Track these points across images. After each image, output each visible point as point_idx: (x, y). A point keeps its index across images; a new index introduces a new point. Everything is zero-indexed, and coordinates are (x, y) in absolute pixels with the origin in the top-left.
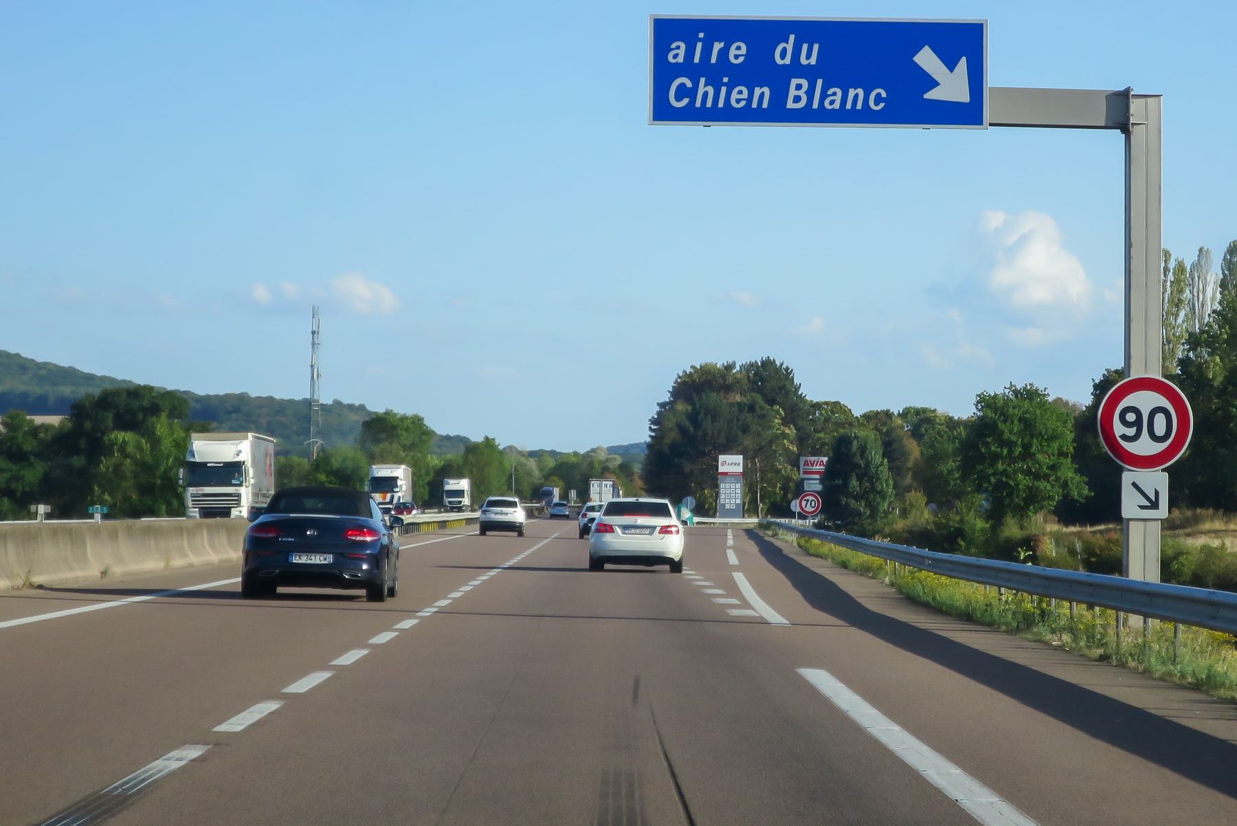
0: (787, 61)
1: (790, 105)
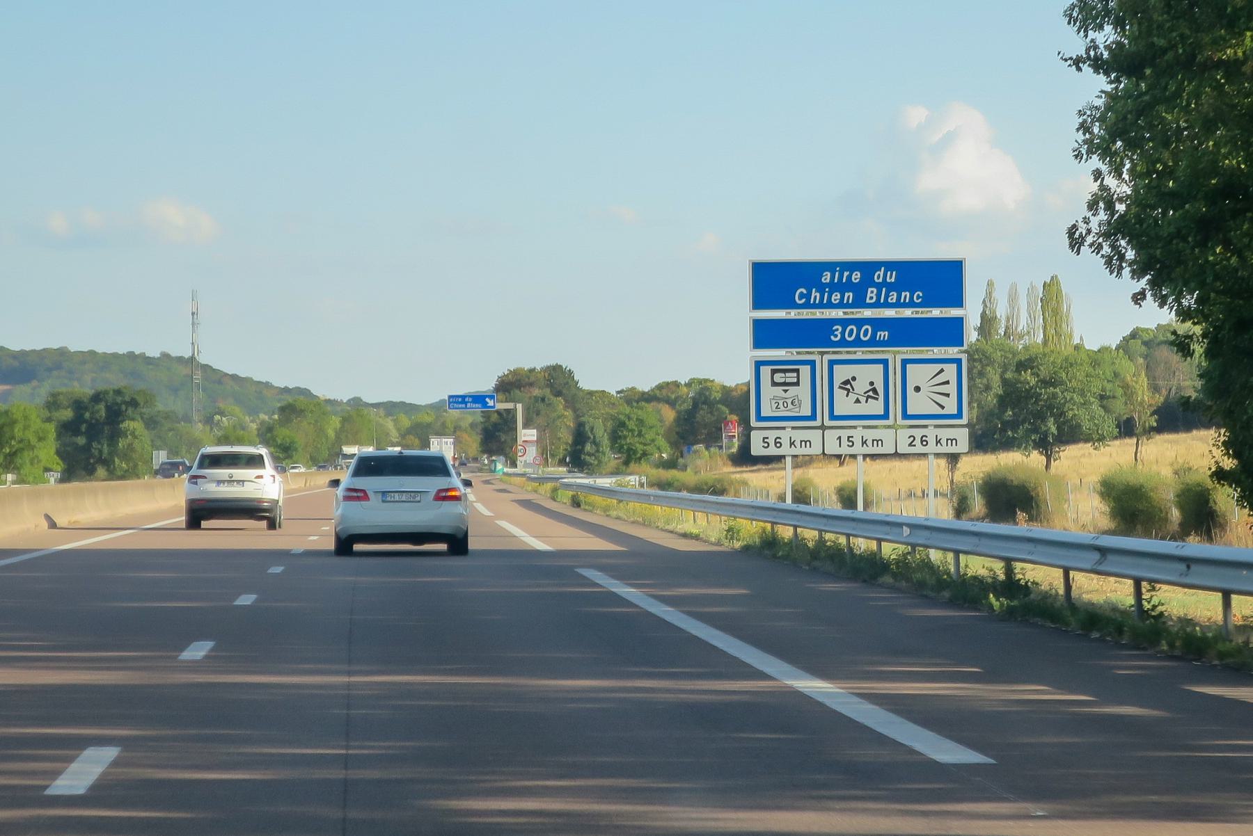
1: (868, 301)
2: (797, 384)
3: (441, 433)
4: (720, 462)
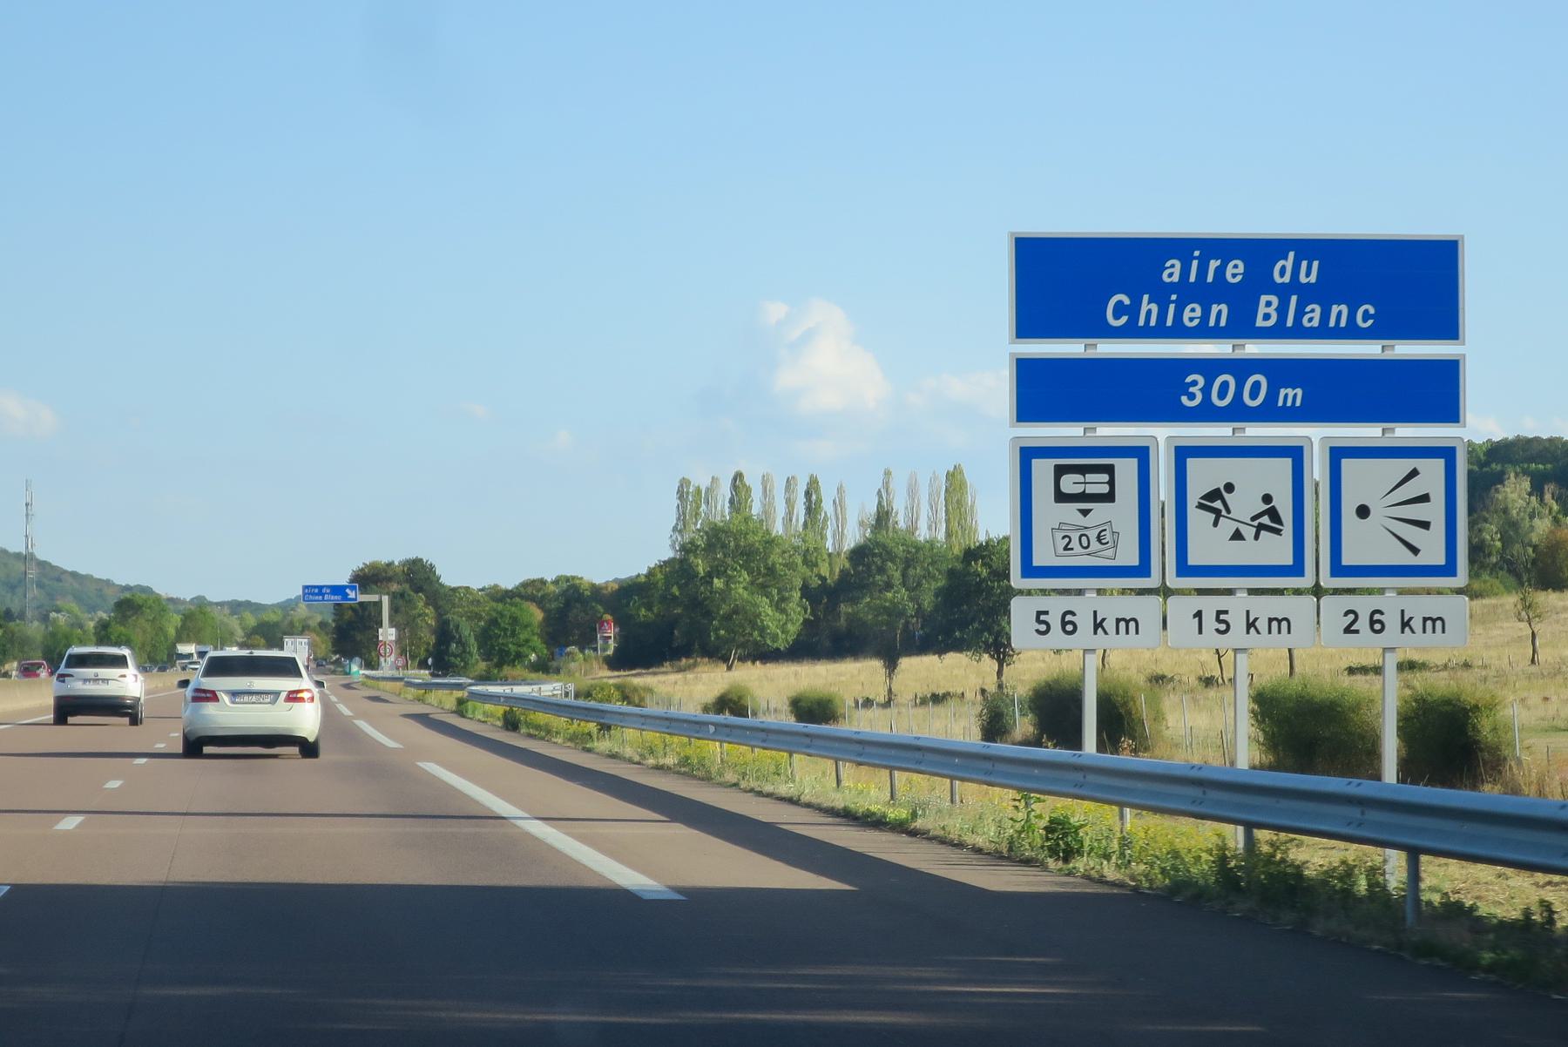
0: (1287, 279)
1: (1260, 323)
2: (1109, 497)
3: (292, 631)
4: (595, 665)
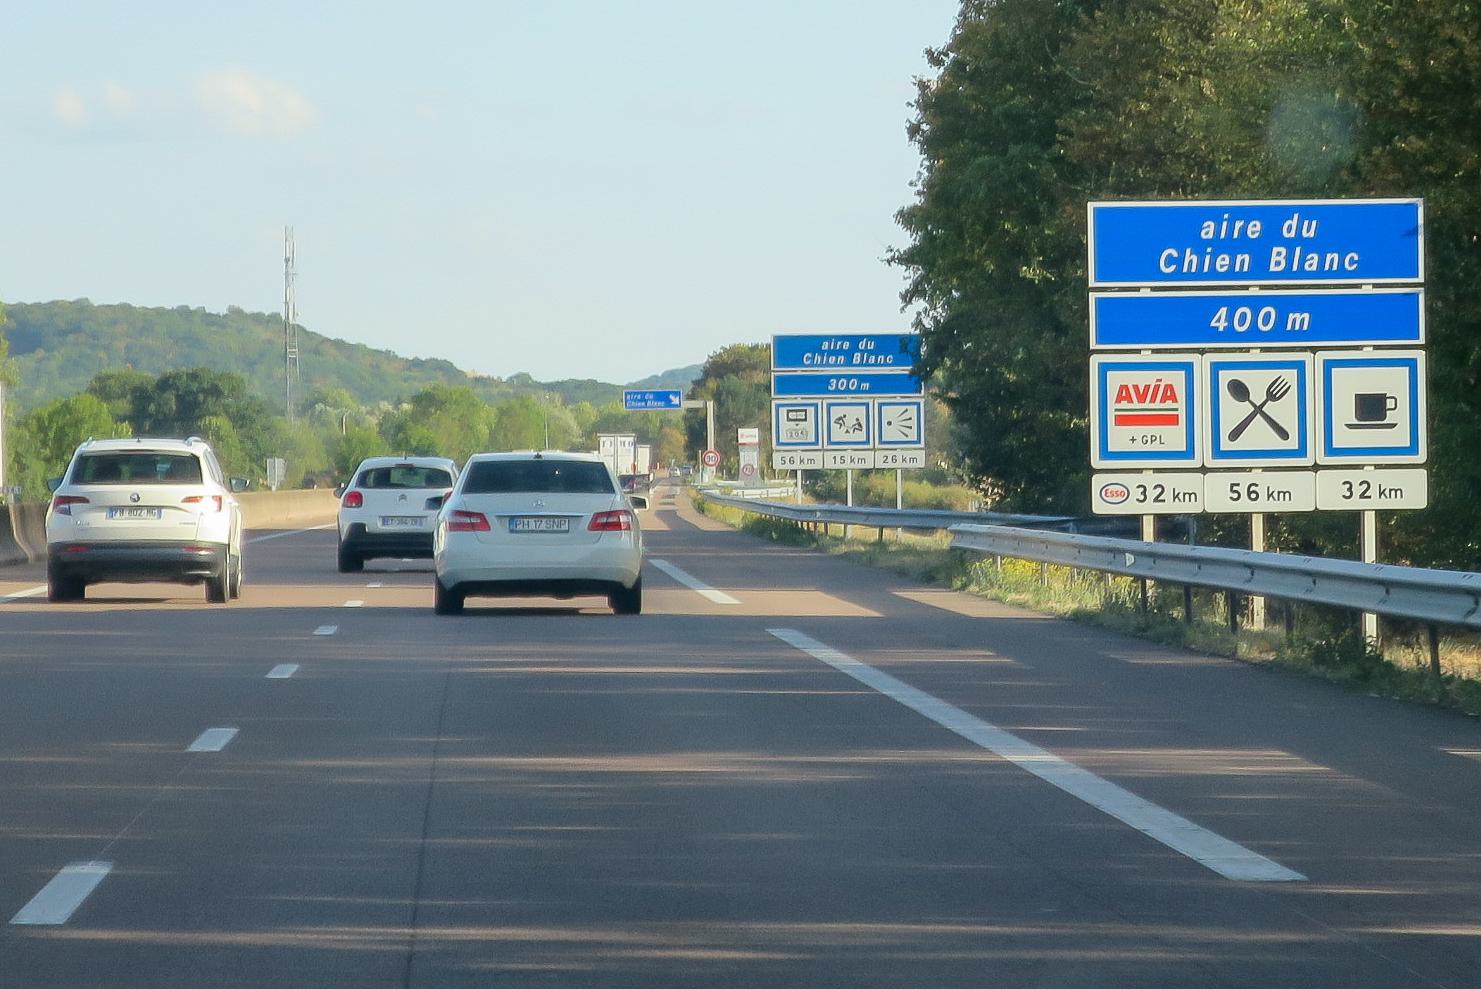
0: (1292, 234)
1: (1273, 268)
2: (805, 420)
